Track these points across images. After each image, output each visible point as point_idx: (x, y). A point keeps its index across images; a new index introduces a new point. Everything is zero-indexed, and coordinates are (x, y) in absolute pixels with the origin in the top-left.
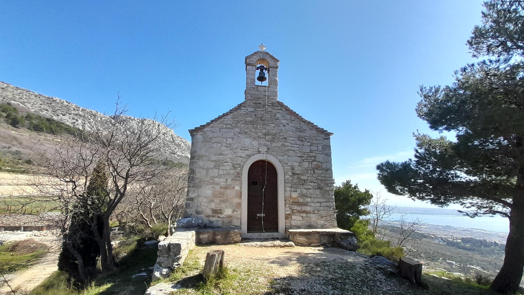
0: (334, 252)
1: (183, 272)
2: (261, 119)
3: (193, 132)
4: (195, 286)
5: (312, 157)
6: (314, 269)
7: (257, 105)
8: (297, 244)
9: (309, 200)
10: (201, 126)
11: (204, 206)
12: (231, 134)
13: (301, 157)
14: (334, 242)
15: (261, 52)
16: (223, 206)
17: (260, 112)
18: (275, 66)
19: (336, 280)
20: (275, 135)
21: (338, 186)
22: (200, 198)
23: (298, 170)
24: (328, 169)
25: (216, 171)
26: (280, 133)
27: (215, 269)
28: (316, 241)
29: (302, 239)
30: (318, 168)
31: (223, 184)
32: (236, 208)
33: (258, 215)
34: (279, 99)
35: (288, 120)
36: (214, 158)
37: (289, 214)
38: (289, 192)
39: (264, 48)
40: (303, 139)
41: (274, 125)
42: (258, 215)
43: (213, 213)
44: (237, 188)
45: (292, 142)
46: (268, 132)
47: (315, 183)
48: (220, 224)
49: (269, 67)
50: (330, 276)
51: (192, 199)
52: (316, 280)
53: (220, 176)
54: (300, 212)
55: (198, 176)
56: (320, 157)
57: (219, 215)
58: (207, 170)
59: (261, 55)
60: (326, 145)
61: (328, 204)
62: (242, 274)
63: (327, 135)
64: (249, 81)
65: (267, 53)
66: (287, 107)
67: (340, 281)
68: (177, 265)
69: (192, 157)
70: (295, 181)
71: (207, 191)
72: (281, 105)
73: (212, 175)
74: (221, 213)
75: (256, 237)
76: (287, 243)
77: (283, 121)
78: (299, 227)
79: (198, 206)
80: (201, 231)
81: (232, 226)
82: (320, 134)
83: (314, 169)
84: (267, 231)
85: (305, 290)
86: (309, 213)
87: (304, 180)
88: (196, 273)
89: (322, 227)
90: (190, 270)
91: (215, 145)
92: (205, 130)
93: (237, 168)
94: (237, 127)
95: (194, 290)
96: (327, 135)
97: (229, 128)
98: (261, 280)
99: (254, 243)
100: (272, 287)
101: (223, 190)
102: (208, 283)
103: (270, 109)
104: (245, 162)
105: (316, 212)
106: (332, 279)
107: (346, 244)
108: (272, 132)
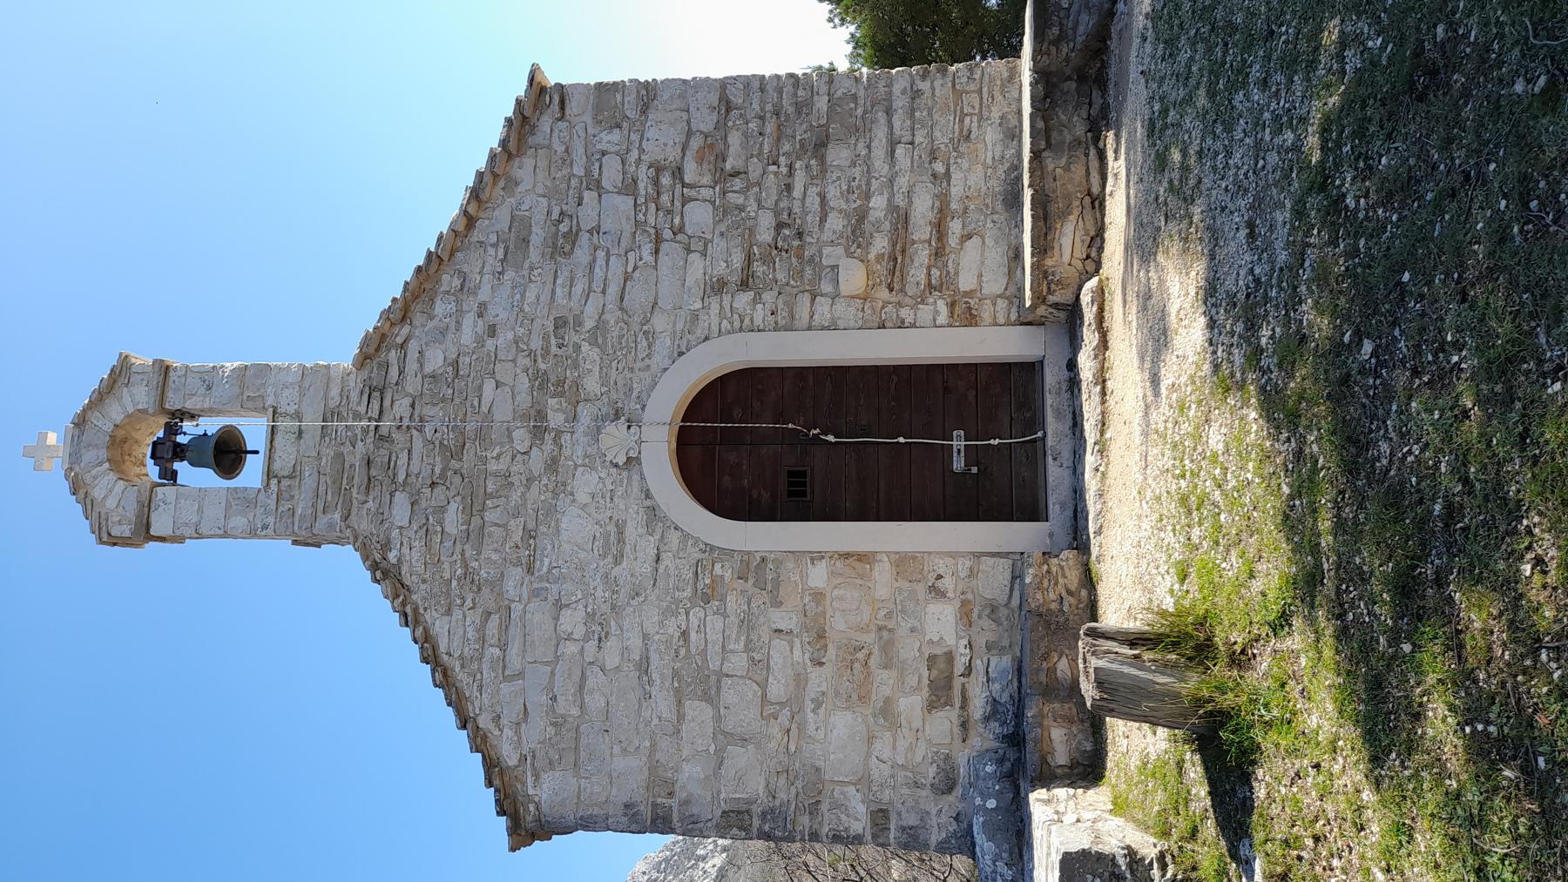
0: (1123, 74)
1: (1194, 834)
2: (457, 453)
3: (526, 827)
4: (1239, 766)
5: (656, 182)
6: (1176, 175)
7: (377, 475)
8: (1090, 267)
9: (878, 203)
10: (489, 784)
11: (911, 748)
12: (538, 615)
13: (658, 240)
14: (1082, 78)
15: (74, 457)
16: (909, 650)
17: (416, 460)
18: (156, 379)
19: (1215, 70)
20: (541, 381)
21: (849, 48)
22: (875, 774)
23: (726, 259)
24: (726, 105)
25: (729, 696)
26: (531, 354)
27: (1166, 667)
28: (1078, 170)
29: (1069, 239)
30: (714, 153)
31: (797, 652)
32: (922, 577)
33: (958, 464)
34: (344, 355)
35: (460, 312)
36: (663, 703)
37: (952, 306)
38: (841, 306)
39: (52, 439)
40: (563, 228)
41: (489, 386)
42: (958, 464)
43: (949, 703)
44: (818, 576)
45: (579, 288)
46: (525, 417)
47: (791, 167)
48: (1005, 662)
49: (163, 411)
50: (1202, 100)
51: (880, 817)
52: (1214, 168)
53: (760, 666)
54: (939, 254)
55: (755, 787)
56: (662, 139)
57: (959, 668)
58: (726, 737)
59: (88, 456)
60: (598, 109)
61: (900, 102)
62: (1196, 533)
63: (541, 101)
64: (239, 522)
65: (81, 422)
66: (386, 315)
67: (1219, 51)
68: (1164, 867)
69: (660, 823)
70: (781, 276)
71: (837, 738)
72: (374, 348)
73: (754, 712)
74: (950, 657)
75: (1067, 473)
76: (1089, 314)
77: (467, 336)
78: (1017, 255)
79: (917, 785)
80: (1031, 758)
81: (1015, 602)
82: (539, 138)
83: (723, 177)
84: (1035, 421)
85: (1251, 225)
86: (943, 200)
87: (780, 226)
88: (1195, 771)
89: (1014, 135)
90: (1187, 802)
91: (595, 702)
92: (512, 761)
93: (717, 581)
94: (497, 583)
95: (1260, 773)
96: (541, 101)
97: (505, 627)
98: (1215, 439)
99: (1091, 482)
100: (1242, 386)
101: (832, 651)
102: (1228, 700)
103: (402, 407)
104: (686, 536)
105: (939, 167)
106: (1212, 94)
107: (1084, 17)
108: (524, 400)
